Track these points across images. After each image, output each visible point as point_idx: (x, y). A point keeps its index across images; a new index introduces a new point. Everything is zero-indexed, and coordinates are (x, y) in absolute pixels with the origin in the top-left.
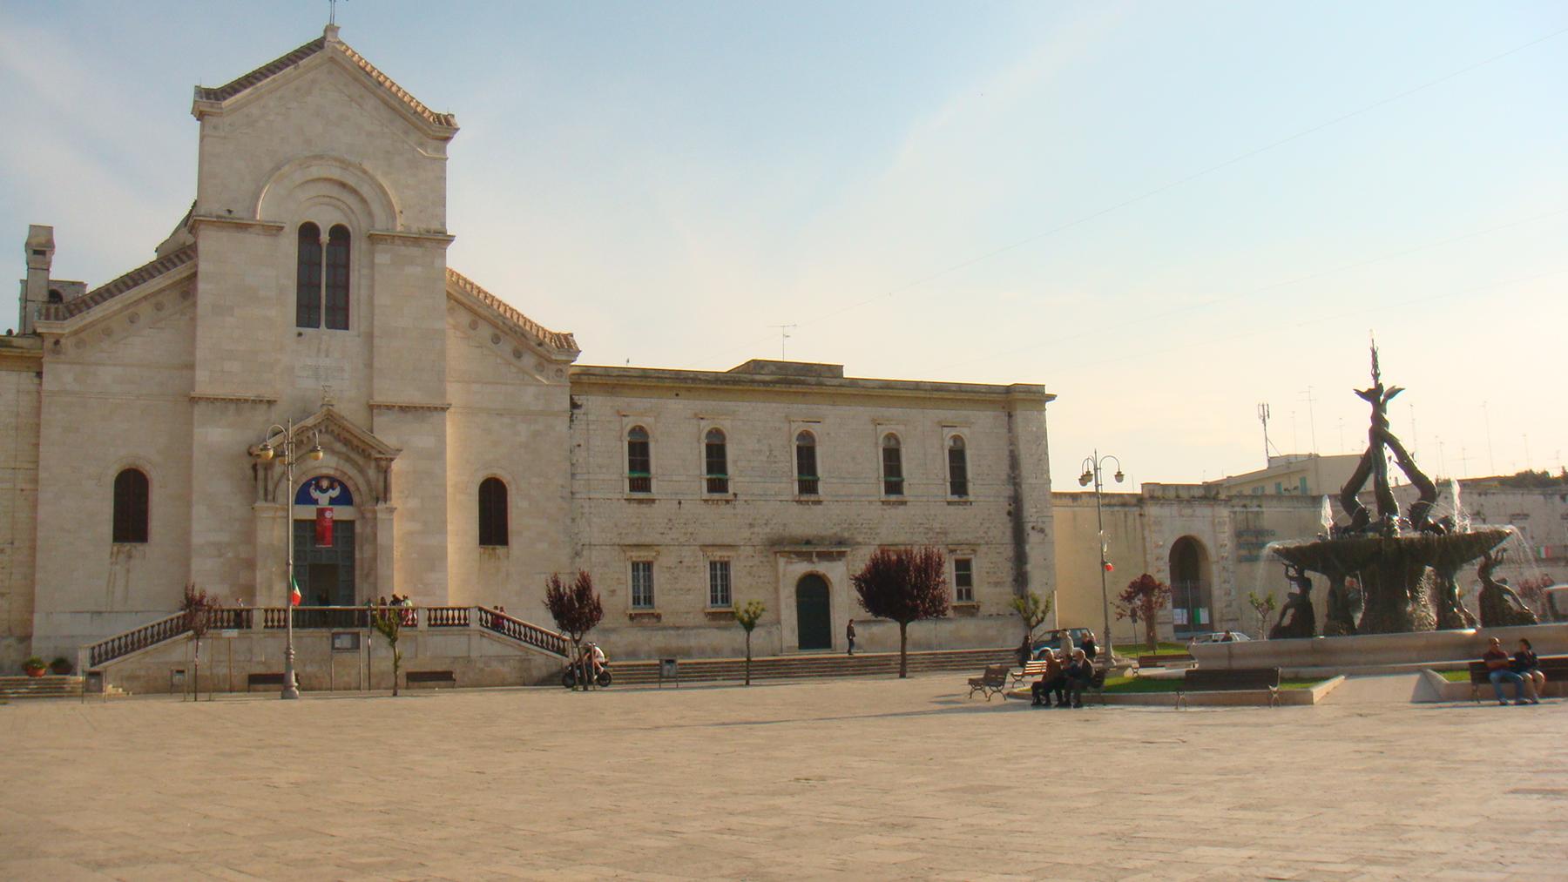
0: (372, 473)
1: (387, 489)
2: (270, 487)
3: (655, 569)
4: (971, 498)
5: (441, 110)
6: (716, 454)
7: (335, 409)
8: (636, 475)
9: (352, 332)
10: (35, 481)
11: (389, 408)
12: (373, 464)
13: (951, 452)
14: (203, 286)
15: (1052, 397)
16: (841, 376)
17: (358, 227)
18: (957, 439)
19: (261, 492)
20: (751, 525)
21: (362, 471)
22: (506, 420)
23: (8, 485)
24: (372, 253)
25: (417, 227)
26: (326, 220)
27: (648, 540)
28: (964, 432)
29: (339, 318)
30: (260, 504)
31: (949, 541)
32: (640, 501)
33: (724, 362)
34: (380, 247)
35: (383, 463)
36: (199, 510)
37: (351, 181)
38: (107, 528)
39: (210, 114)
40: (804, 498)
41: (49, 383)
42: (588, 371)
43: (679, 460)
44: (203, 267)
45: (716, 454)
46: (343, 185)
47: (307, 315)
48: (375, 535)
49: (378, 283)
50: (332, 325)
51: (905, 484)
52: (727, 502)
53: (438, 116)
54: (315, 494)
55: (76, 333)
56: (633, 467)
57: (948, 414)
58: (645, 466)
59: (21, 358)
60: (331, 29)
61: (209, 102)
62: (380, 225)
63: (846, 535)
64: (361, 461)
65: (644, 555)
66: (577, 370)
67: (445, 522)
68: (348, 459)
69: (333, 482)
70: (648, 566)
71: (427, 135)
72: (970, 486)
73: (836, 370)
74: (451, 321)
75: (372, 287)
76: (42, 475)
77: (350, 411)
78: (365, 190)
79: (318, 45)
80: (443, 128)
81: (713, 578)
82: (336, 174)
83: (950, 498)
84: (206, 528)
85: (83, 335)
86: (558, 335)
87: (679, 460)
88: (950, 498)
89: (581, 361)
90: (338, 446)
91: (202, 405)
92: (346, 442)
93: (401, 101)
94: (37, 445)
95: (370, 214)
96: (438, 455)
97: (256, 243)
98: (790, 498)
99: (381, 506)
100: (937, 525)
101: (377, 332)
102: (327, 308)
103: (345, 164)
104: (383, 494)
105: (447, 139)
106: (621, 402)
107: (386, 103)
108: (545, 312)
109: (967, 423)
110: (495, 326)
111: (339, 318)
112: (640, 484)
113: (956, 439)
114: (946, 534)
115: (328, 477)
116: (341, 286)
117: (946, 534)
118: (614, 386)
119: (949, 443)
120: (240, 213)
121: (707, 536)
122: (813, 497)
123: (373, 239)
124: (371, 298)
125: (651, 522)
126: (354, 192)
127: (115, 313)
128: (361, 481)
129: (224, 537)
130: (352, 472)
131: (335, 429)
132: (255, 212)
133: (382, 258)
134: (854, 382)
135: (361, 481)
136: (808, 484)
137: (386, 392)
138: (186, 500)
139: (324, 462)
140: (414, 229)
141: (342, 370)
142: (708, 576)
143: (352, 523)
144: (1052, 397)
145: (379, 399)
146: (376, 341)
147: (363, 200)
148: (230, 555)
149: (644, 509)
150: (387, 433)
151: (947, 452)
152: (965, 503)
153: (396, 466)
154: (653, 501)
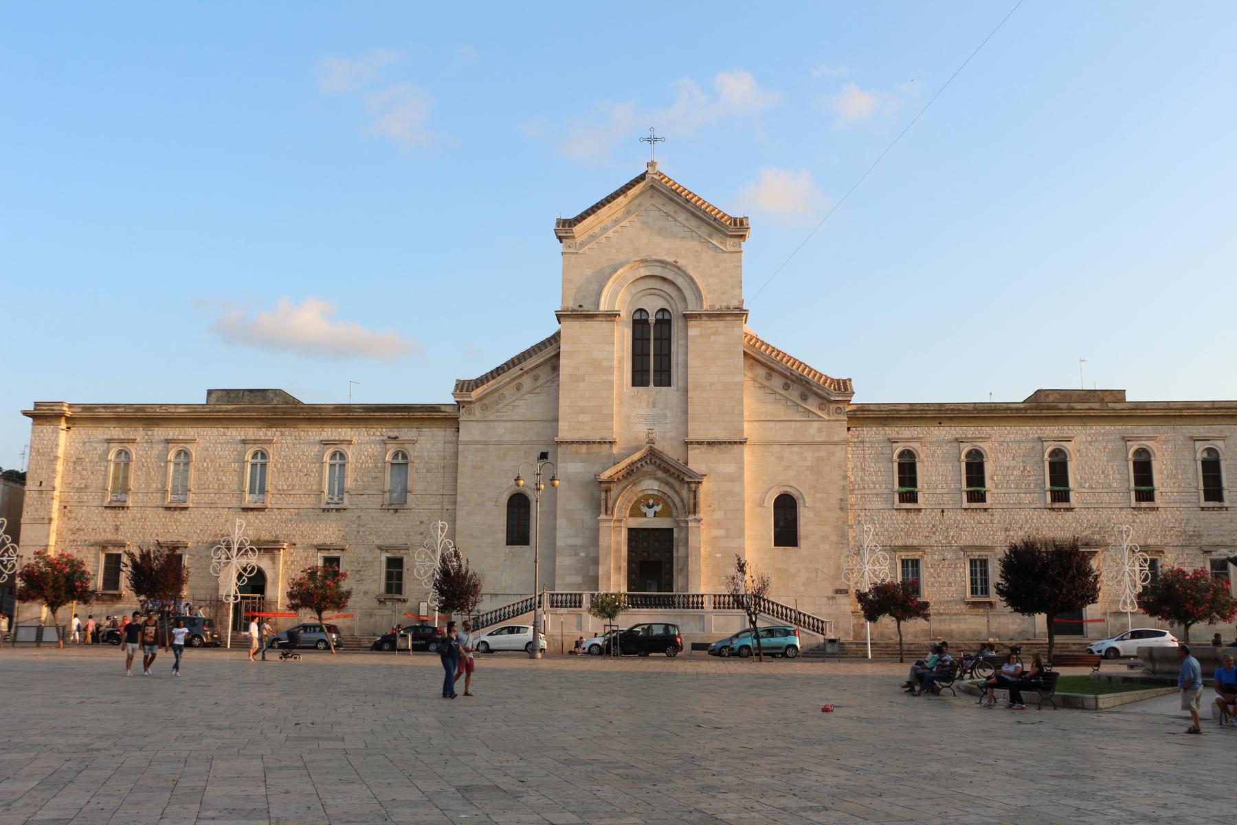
0: (684, 493)
1: (695, 505)
2: (610, 505)
3: (922, 564)
4: (1226, 504)
5: (738, 215)
6: (975, 470)
7: (655, 446)
8: (904, 489)
9: (673, 388)
10: (455, 503)
11: (701, 443)
12: (686, 486)
13: (1204, 463)
14: (563, 361)
15: (25, 413)
16: (1123, 400)
17: (677, 309)
18: (1057, 453)
19: (603, 509)
20: (1007, 530)
21: (677, 493)
22: (795, 449)
23: (438, 507)
24: (686, 328)
25: (719, 304)
26: (652, 306)
27: (916, 543)
28: (1219, 445)
29: (664, 379)
30: (602, 517)
31: (1204, 542)
32: (908, 510)
33: (1017, 393)
34: (691, 323)
35: (693, 486)
36: (561, 522)
37: (669, 276)
38: (502, 536)
39: (566, 237)
40: (1057, 505)
41: (464, 435)
42: (863, 408)
43: (939, 474)
44: (564, 348)
45: (975, 470)
46: (664, 279)
47: (639, 378)
48: (687, 539)
49: (702, 354)
50: (658, 384)
51: (1157, 494)
52: (985, 510)
53: (735, 220)
54: (645, 509)
55: (480, 399)
56: (902, 483)
57: (1201, 430)
58: (1149, 481)
59: (445, 419)
60: (651, 164)
61: (565, 228)
62: (692, 308)
63: (1097, 537)
64: (677, 485)
65: (912, 555)
66: (853, 407)
67: (743, 530)
68: (667, 483)
69: (657, 500)
70: (916, 563)
71: (727, 236)
72: (1225, 493)
73: (1119, 395)
74: (749, 374)
75: (686, 354)
76: (459, 499)
77: (670, 450)
78: (680, 281)
79: (642, 177)
80: (737, 229)
81: (973, 573)
82: (658, 271)
83: (1203, 504)
84: (565, 536)
85: (485, 401)
86: (838, 381)
87: (939, 474)
88: (1203, 504)
89: (854, 400)
90: (660, 474)
91: (563, 446)
92: (666, 471)
93: (699, 208)
94: (456, 479)
95: (684, 299)
96: (738, 478)
97: (598, 327)
98: (309, 502)
99: (691, 517)
100: (1190, 529)
101: (690, 387)
102: (649, 371)
103: (664, 264)
104: (695, 509)
105: (742, 237)
106: (891, 431)
107: (693, 214)
108: (826, 363)
109: (984, 439)
110: (785, 376)
111: (664, 379)
112: (977, 496)
113: (1210, 450)
114: (1199, 536)
115: (652, 496)
116: (664, 356)
117: (1199, 536)
118: (886, 419)
119: (1201, 455)
120: (588, 307)
121: (966, 540)
122: (1065, 505)
123: (686, 317)
124: (686, 362)
125: (918, 527)
126: (672, 283)
127: (507, 384)
128: (677, 499)
129: (578, 541)
130: (670, 493)
131: (654, 459)
132: (598, 305)
133: (694, 330)
134: (1138, 406)
135: (677, 499)
136: (1060, 494)
137: (697, 431)
138: (552, 514)
139: (650, 485)
140: (717, 307)
141: (665, 416)
142: (968, 572)
143: (671, 530)
144: (25, 413)
145: (692, 437)
146: (690, 394)
147: (679, 289)
148: (582, 554)
149: (912, 515)
150: (698, 462)
151: (1199, 464)
152: (1221, 508)
153: (703, 489)
154: (920, 510)
